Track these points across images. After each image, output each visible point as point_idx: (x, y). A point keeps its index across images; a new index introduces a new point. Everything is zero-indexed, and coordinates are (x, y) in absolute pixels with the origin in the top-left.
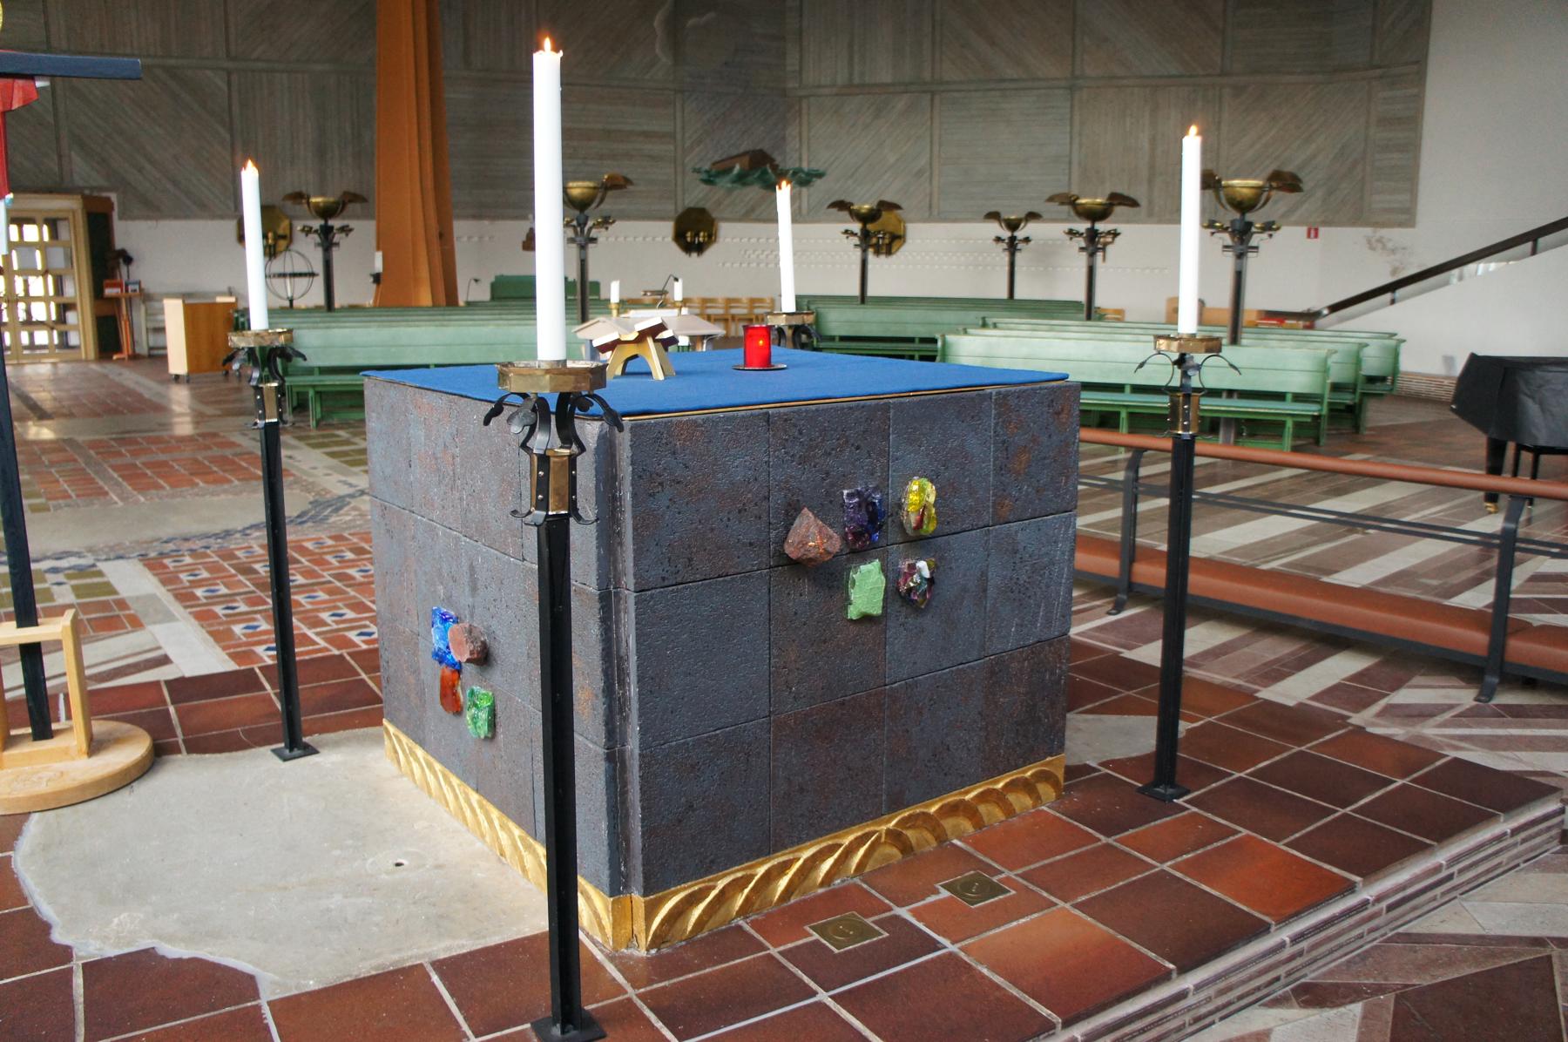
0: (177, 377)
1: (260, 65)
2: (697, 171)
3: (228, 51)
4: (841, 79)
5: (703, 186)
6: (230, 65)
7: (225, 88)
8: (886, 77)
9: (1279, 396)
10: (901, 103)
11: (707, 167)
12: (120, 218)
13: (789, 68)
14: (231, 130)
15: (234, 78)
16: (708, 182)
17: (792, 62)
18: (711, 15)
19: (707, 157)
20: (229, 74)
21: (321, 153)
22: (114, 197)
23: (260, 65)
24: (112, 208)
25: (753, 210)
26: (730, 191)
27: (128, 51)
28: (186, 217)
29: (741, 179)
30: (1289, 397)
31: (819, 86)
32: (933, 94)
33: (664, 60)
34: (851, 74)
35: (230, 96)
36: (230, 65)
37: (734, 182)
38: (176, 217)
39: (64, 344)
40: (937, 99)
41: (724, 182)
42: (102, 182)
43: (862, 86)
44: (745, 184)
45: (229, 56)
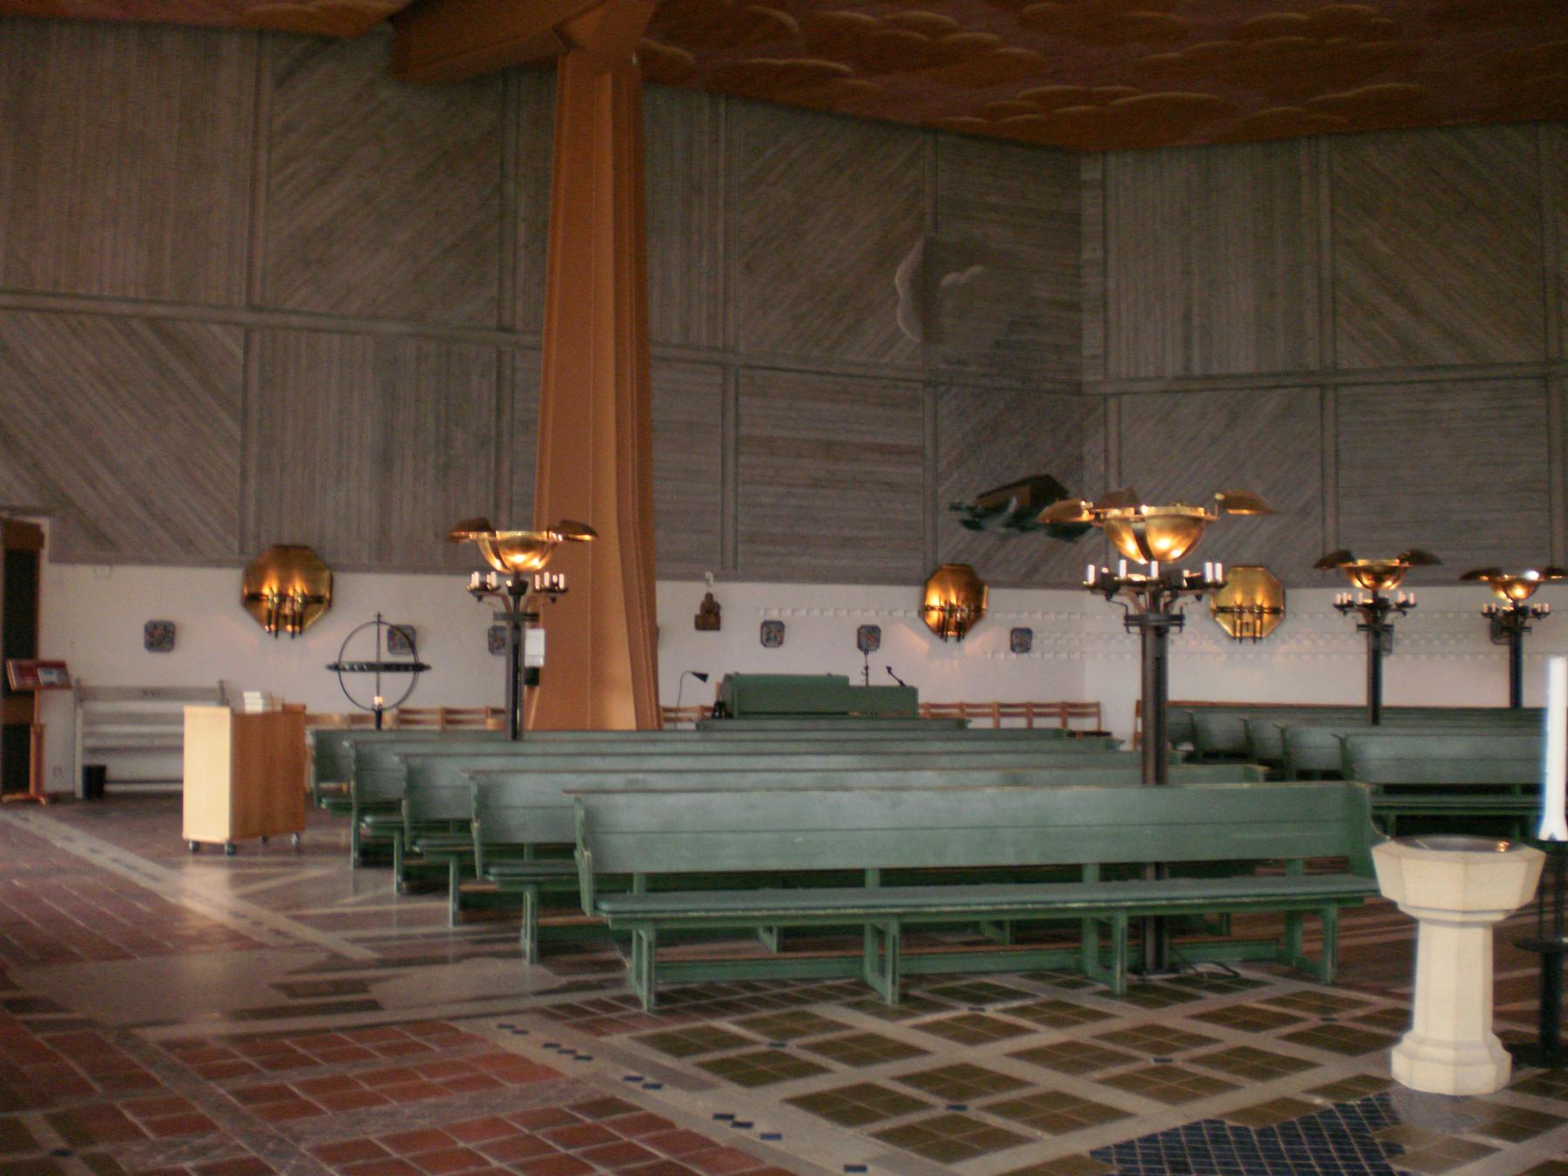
0: (198, 847)
1: (296, 320)
2: (956, 508)
3: (249, 293)
4: (1172, 368)
5: (965, 531)
6: (250, 318)
7: (239, 353)
8: (1243, 363)
9: (851, 878)
10: (1271, 404)
11: (970, 502)
12: (54, 559)
13: (1086, 353)
14: (244, 426)
15: (256, 337)
16: (972, 525)
17: (1091, 342)
18: (976, 270)
19: (967, 487)
20: (249, 332)
21: (385, 462)
22: (45, 524)
23: (296, 320)
24: (40, 543)
25: (1035, 569)
26: (1004, 539)
27: (94, 291)
28: (161, 562)
29: (1021, 522)
30: (872, 879)
31: (1137, 380)
32: (1322, 387)
33: (909, 335)
34: (1188, 360)
35: (246, 368)
36: (250, 318)
37: (1008, 525)
38: (145, 561)
39: (1069, 653)
40: (1330, 394)
41: (996, 525)
42: (32, 501)
43: (1208, 377)
44: (1024, 529)
45: (252, 307)
